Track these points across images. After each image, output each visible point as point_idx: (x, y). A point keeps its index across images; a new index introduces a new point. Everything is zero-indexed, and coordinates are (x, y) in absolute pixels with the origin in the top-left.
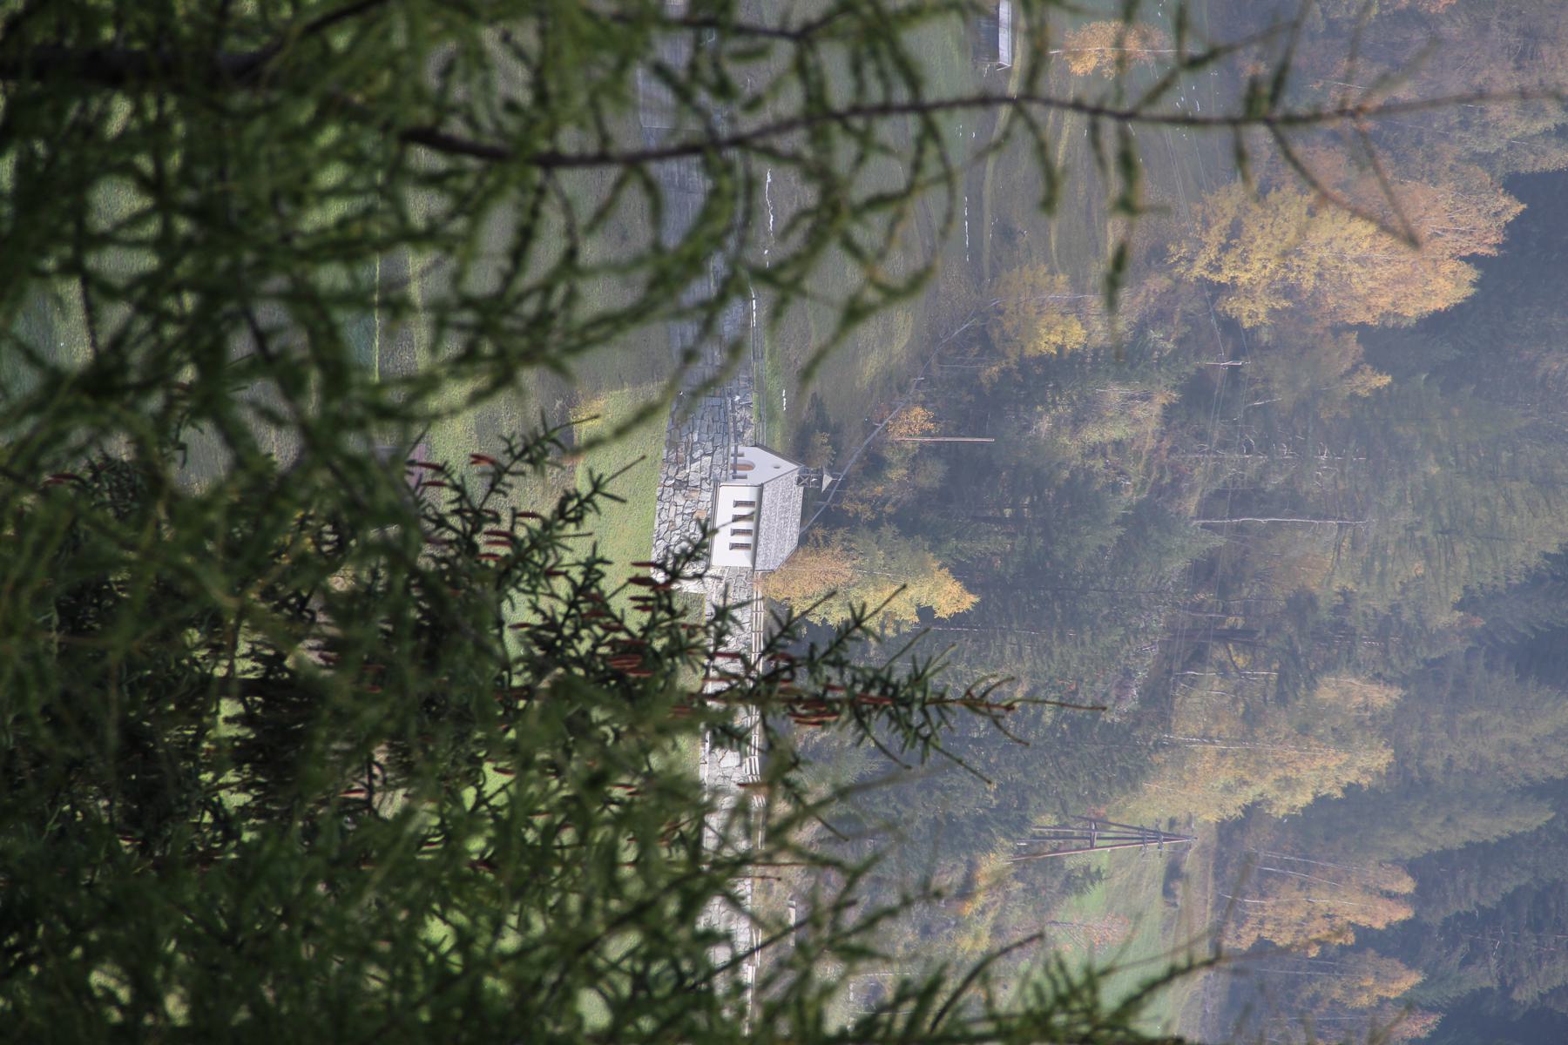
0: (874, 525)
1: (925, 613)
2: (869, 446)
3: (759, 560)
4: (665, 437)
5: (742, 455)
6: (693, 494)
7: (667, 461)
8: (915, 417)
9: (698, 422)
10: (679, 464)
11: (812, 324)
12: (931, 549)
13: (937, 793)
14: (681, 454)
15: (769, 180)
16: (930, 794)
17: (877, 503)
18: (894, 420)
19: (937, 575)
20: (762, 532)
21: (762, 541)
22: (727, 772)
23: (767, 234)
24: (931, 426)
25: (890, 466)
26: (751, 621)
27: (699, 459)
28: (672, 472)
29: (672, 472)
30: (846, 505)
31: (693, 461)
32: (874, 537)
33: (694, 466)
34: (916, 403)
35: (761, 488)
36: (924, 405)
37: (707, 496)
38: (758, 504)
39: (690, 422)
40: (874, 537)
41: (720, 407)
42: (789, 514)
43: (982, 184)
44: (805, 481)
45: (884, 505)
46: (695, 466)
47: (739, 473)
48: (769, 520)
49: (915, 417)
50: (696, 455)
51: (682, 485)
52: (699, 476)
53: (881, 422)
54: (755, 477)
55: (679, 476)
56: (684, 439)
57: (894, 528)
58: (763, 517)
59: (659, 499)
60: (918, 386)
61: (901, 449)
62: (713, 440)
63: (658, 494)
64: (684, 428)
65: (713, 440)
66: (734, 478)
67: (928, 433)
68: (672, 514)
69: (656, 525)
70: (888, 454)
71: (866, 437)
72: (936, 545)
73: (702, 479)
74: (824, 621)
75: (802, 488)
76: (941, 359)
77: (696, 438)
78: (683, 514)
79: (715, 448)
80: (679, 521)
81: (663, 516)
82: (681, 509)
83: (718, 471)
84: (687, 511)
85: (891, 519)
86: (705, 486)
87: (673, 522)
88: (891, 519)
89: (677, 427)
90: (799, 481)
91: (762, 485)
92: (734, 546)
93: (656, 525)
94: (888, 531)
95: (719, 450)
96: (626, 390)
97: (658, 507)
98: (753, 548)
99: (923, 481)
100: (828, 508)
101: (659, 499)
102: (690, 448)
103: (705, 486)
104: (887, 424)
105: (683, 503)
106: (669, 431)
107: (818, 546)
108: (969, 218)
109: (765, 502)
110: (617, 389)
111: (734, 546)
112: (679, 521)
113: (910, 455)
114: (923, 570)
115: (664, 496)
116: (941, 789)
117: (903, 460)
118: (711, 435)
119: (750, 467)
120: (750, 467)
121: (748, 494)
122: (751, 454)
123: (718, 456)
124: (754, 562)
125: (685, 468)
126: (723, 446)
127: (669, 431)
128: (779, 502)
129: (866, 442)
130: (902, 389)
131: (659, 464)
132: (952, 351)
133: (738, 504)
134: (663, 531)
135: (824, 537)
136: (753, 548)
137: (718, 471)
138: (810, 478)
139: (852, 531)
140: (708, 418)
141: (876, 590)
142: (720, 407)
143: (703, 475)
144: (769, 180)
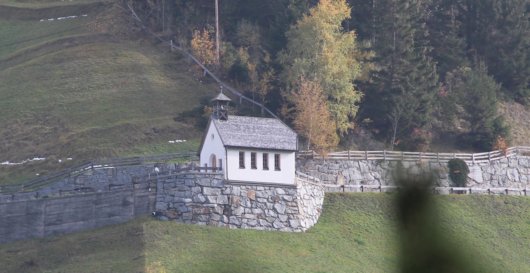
0: (279, 68)
1: (346, 26)
2: (222, 79)
3: (288, 147)
4: (188, 223)
5: (206, 165)
6: (235, 200)
7: (208, 222)
8: (199, 44)
9: (176, 199)
10: (209, 212)
11: (117, 124)
12: (295, 23)
13: (509, 18)
14: (202, 211)
15: (7, 163)
16: (509, 23)
17: (262, 69)
18: (202, 60)
19: (316, 16)
20: (265, 146)
21: (272, 146)
22: (488, 177)
23: (46, 161)
24: (206, 33)
25: (238, 61)
26: (358, 161)
27: (206, 196)
28: (217, 217)
29: (217, 217)
30: (264, 91)
31: (207, 201)
32: (287, 67)
33: (211, 201)
34: (189, 44)
35: (228, 147)
36: (190, 38)
37: (236, 190)
38: (241, 150)
39: (176, 205)
40: (287, 67)
41: (164, 182)
42: (251, 126)
43: (32, 10)
44: (223, 114)
45: (264, 63)
46: (211, 199)
47: (218, 166)
48: (254, 141)
49: (199, 44)
50: (203, 199)
51: (227, 210)
52: (220, 196)
53: (203, 70)
54: (220, 153)
55: (220, 211)
56: (190, 209)
57: (280, 53)
58: (252, 145)
59: (239, 226)
60: (178, 45)
61: (227, 55)
62: (190, 187)
63: (235, 227)
64: (181, 209)
65: (190, 187)
66: (221, 169)
67: (212, 36)
68: (252, 216)
69: (261, 228)
70: (230, 64)
71: (215, 81)
72: (292, 19)
73: (222, 194)
74: (356, 103)
75: (229, 117)
76: (159, 29)
77: (189, 200)
78: (251, 208)
79: (196, 185)
80: (257, 211)
81: (253, 223)
82: (247, 210)
83: (215, 182)
84: (249, 205)
85: (274, 57)
86: (228, 191)
87: (259, 216)
88: (274, 57)
89: (181, 215)
90: (223, 119)
91: (225, 146)
92: (277, 167)
93: (261, 228)
94: (282, 57)
95: (198, 182)
96: (146, 254)
97: (246, 227)
98: (278, 152)
99: (254, 38)
100: (267, 105)
101: (239, 226)
102: (197, 204)
103: (228, 191)
104: (205, 66)
105: (242, 208)
106: (184, 221)
107: (295, 111)
108: (55, 17)
109: (239, 144)
110: (144, 261)
111: (277, 167)
112: (257, 211)
113: (232, 48)
114: (311, 28)
115: (237, 223)
116: (505, 15)
117: (235, 53)
118: (186, 188)
119: (214, 158)
120: (214, 158)
121: (234, 158)
122: (205, 159)
123: (203, 182)
124: (290, 151)
125: (213, 208)
126: (195, 179)
127: (184, 221)
128: (239, 134)
129: (218, 80)
130: (179, 56)
131: (209, 227)
132: (152, 21)
133: (242, 165)
134: (266, 223)
135: (289, 107)
136: (278, 152)
137: (215, 182)
138: (221, 110)
139: (284, 85)
140: (173, 191)
141: (327, 63)
142: (164, 182)
143: (219, 193)
144: (7, 163)
